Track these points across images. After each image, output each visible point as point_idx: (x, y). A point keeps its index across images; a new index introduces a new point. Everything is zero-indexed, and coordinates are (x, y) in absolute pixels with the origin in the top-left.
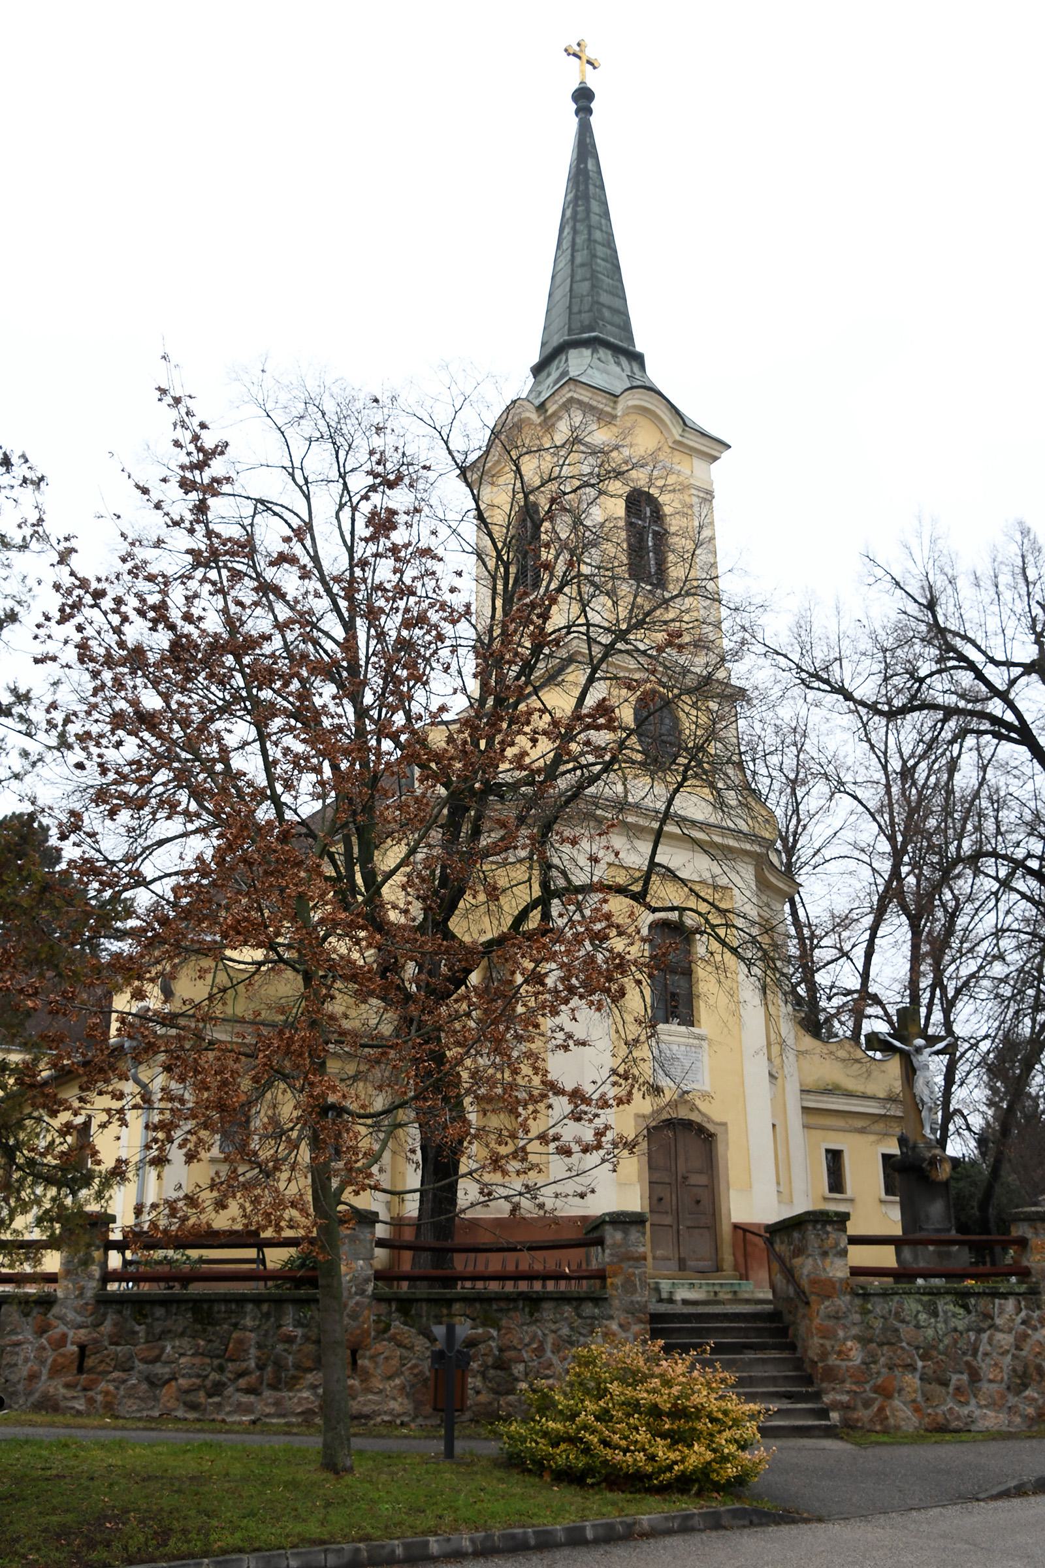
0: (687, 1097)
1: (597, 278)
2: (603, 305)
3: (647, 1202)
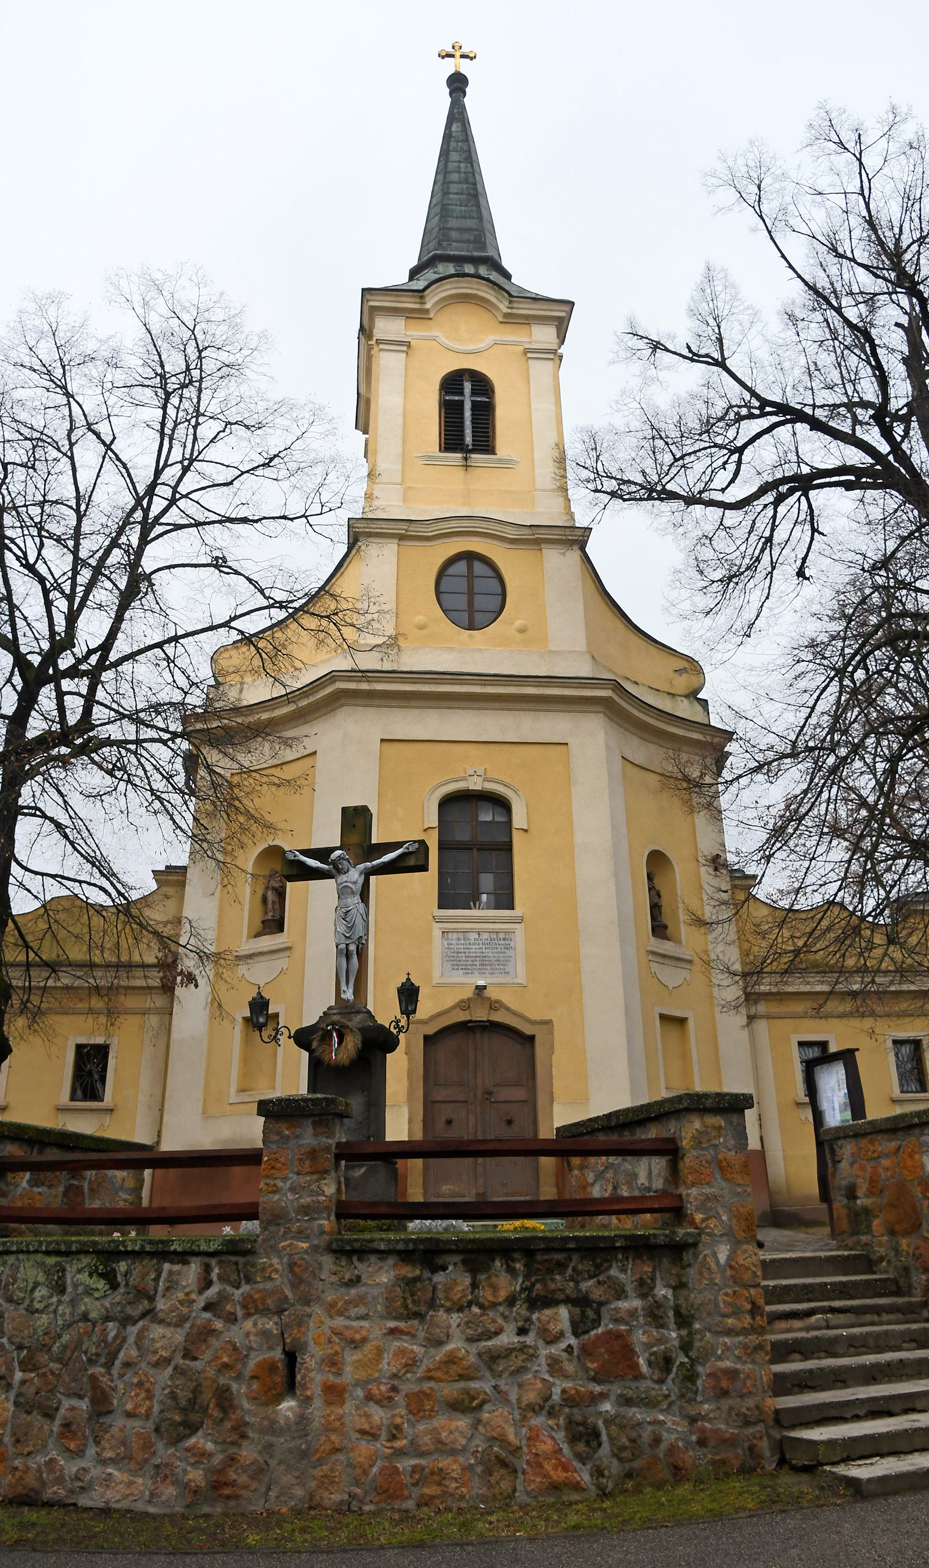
3: (419, 1126)
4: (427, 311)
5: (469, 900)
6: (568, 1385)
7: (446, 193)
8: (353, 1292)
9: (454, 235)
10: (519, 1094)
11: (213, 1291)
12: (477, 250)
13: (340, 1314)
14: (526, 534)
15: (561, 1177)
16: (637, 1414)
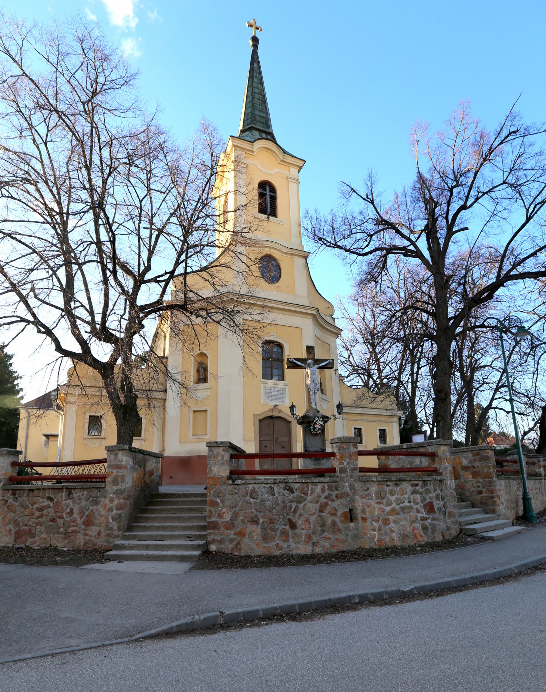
0: (278, 407)
1: (254, 106)
2: (256, 115)
3: (258, 448)
4: (253, 152)
5: (271, 377)
6: (421, 515)
7: (253, 98)
8: (367, 492)
9: (258, 118)
10: (286, 439)
11: (326, 493)
12: (266, 128)
13: (364, 498)
14: (289, 251)
15: (261, 464)
16: (435, 522)
